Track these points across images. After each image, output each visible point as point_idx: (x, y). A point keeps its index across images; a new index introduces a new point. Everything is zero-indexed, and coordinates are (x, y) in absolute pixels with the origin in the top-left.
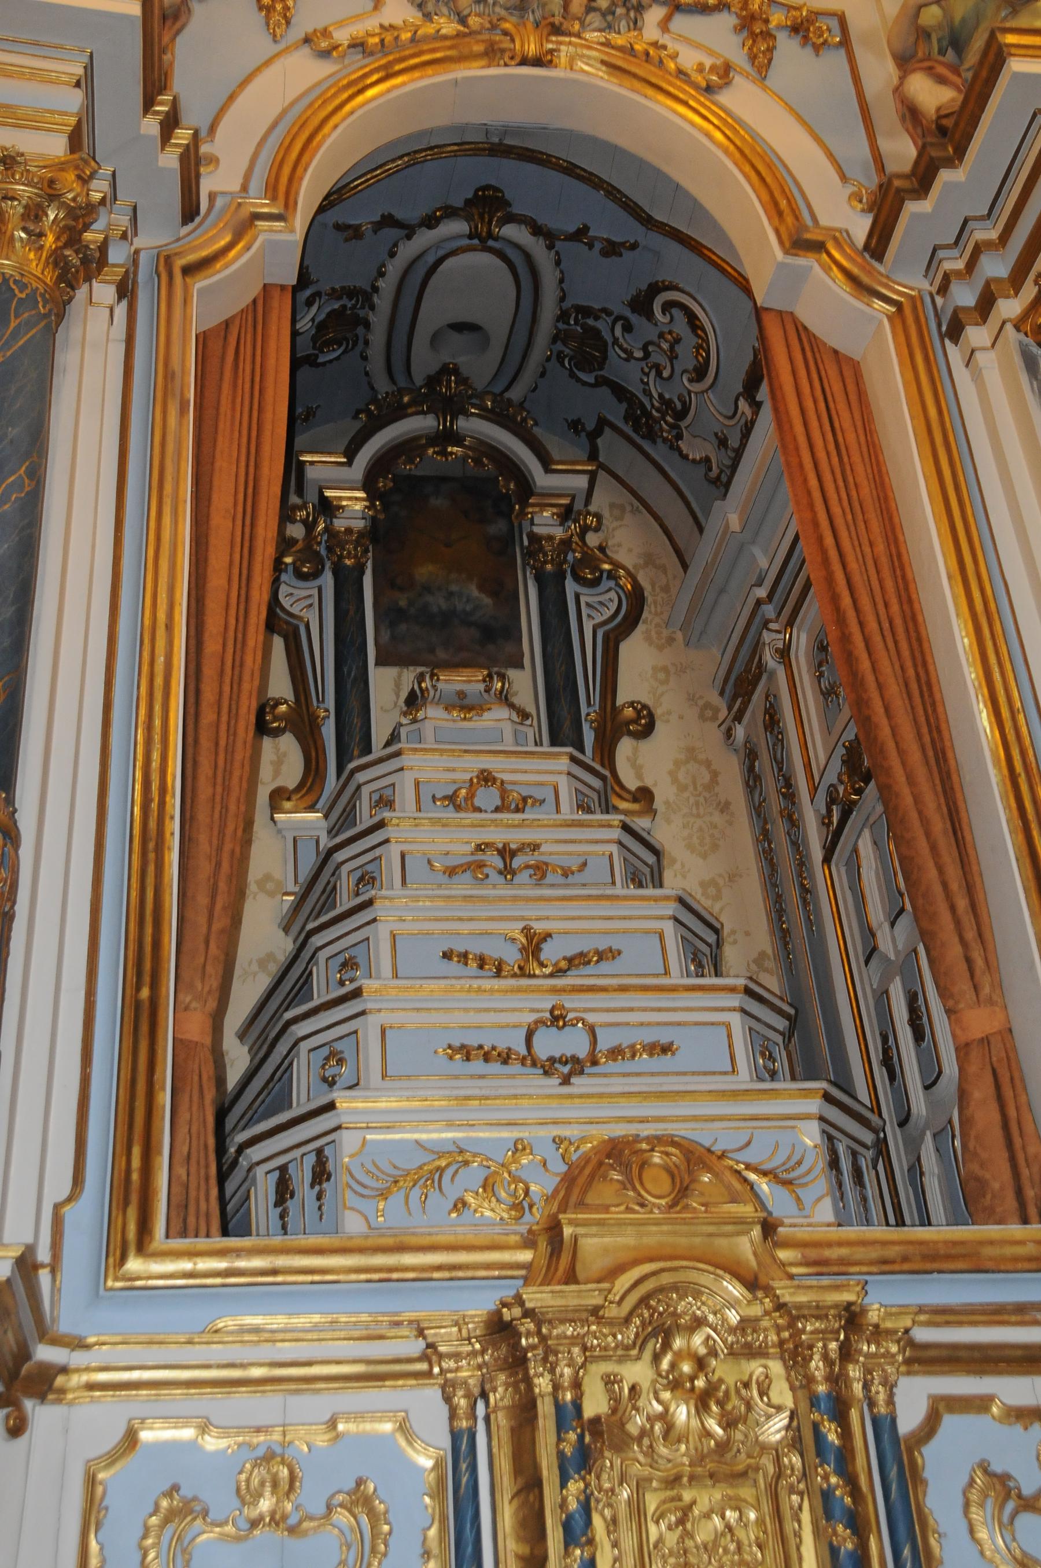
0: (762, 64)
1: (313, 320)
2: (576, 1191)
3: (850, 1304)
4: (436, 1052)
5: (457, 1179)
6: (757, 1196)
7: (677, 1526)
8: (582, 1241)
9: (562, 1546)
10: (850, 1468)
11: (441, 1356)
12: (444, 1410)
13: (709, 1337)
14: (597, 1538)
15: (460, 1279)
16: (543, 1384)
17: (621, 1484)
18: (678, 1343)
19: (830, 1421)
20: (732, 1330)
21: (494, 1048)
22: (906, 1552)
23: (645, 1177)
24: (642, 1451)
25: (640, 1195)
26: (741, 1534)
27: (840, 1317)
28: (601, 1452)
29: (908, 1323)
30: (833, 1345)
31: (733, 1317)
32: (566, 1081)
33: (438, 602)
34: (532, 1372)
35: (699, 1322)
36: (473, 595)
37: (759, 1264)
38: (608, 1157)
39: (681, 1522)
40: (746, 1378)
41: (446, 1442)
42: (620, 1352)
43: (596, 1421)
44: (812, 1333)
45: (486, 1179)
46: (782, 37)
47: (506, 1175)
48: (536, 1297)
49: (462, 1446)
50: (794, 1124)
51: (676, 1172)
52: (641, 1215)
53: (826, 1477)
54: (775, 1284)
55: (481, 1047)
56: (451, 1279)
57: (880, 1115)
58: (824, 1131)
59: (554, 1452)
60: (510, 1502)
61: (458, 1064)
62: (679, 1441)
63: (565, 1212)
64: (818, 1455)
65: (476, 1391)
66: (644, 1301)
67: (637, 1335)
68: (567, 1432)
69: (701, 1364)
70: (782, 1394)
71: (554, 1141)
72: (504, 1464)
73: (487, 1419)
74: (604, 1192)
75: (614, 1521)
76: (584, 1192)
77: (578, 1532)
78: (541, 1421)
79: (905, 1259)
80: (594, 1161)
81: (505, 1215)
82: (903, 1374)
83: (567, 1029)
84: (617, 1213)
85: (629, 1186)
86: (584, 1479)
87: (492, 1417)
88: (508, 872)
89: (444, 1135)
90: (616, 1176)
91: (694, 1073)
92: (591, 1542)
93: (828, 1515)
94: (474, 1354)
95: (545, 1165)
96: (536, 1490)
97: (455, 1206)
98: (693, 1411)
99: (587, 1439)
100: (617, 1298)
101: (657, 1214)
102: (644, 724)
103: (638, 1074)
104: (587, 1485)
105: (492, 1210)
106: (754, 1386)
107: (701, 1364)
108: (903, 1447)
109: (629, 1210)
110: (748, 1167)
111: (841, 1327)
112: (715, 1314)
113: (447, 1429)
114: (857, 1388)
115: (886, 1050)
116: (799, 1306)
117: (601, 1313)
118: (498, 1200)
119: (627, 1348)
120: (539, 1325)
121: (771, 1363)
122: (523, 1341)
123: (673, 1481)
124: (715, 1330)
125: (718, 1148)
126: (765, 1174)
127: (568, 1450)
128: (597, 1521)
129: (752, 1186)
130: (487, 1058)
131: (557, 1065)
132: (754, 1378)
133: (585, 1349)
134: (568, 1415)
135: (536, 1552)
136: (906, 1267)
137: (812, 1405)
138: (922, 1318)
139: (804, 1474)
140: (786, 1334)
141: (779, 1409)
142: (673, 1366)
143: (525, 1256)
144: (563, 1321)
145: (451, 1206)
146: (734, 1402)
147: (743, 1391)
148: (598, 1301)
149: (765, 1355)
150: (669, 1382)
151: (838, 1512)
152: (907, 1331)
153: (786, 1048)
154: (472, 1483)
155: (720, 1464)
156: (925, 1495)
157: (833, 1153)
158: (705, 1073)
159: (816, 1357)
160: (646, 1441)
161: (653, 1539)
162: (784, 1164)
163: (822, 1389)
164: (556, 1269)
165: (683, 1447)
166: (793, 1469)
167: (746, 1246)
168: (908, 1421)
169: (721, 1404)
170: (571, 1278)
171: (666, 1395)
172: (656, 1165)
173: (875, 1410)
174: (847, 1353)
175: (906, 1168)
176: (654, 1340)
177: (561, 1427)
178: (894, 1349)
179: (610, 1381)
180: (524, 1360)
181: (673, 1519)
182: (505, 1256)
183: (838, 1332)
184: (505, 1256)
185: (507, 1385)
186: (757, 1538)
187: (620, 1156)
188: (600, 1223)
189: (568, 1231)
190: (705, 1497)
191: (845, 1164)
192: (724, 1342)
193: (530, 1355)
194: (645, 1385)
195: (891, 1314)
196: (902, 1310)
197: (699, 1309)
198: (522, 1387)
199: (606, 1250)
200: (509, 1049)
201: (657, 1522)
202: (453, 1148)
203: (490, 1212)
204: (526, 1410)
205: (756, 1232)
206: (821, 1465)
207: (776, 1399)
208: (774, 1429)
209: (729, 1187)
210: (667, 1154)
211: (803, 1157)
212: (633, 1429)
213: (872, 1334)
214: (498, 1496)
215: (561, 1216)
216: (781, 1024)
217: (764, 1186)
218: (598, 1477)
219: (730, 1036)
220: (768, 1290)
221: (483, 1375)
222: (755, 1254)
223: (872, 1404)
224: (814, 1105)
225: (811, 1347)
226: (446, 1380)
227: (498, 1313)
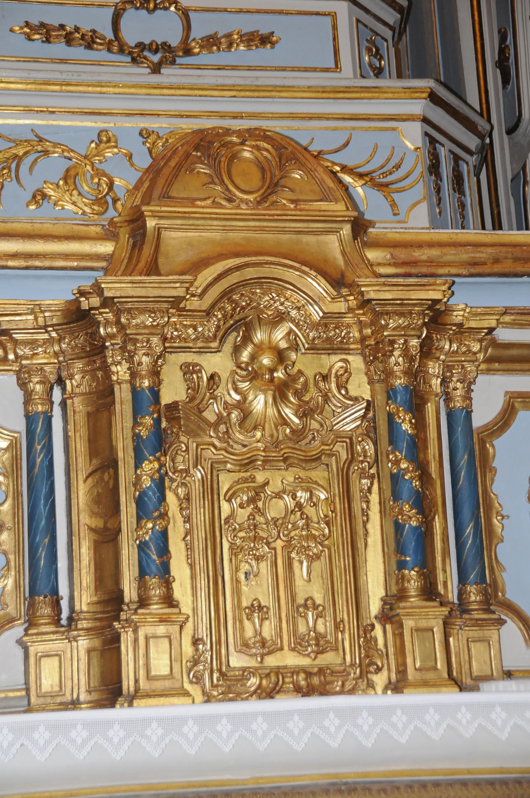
2: (161, 181)
3: (436, 302)
4: (12, 30)
5: (36, 168)
6: (350, 197)
7: (248, 505)
8: (165, 234)
9: (134, 521)
10: (421, 456)
11: (16, 342)
12: (20, 395)
13: (291, 331)
14: (170, 514)
15: (37, 268)
16: (121, 371)
17: (195, 466)
18: (259, 336)
19: (406, 412)
20: (315, 326)
21: (77, 29)
22: (469, 530)
23: (233, 171)
24: (218, 438)
25: (228, 189)
26: (310, 511)
27: (425, 315)
28: (177, 435)
29: (493, 324)
30: (414, 342)
31: (315, 313)
32: (156, 69)
34: (110, 360)
35: (281, 318)
37: (346, 262)
38: (197, 148)
39: (252, 500)
40: (325, 372)
41: (21, 425)
42: (200, 344)
43: (173, 407)
44: (395, 329)
45: (68, 171)
47: (89, 168)
48: (116, 287)
49: (37, 428)
50: (395, 124)
51: (267, 168)
52: (228, 209)
53: (397, 462)
54: (362, 281)
55: (62, 27)
56: (27, 268)
57: (489, 120)
58: (426, 134)
59: (130, 435)
60: (85, 481)
61: (37, 47)
62: (255, 428)
63: (148, 204)
64: (391, 442)
65: (53, 378)
66: (226, 294)
67: (218, 327)
68: (143, 417)
69: (281, 356)
70: (360, 387)
71: (141, 134)
72: (80, 446)
73: (63, 404)
74: (187, 186)
75: (188, 498)
76: (169, 184)
77: (151, 507)
78: (118, 406)
79: (497, 261)
80: (181, 152)
81: (87, 210)
82: (483, 372)
83: (158, 12)
84: (204, 207)
85: (216, 180)
86: (158, 460)
87: (69, 402)
89: (21, 122)
90: (202, 169)
91: (293, 69)
92: (164, 516)
93: (396, 496)
94: (51, 341)
95: (130, 157)
96: (111, 471)
97: (34, 197)
98: (270, 400)
99: (164, 424)
100: (199, 291)
101: (244, 209)
103: (234, 68)
104: (162, 465)
105: (74, 203)
106: (333, 379)
107: (281, 356)
108: (475, 440)
109: (216, 204)
110: (344, 169)
111: (425, 324)
112: (298, 309)
113: (22, 412)
114: (436, 383)
115: (503, 51)
116: (384, 302)
117: (182, 305)
118: (80, 194)
119: (208, 340)
120: (118, 314)
121: (350, 358)
122: (102, 330)
123: (248, 464)
124: (297, 325)
125: (314, 148)
126: (361, 176)
127: (144, 433)
128: (170, 497)
129: (346, 188)
130: (69, 40)
131: (146, 53)
132: (334, 371)
133: (165, 339)
134: (145, 400)
135: (109, 525)
136: (497, 268)
137: (389, 398)
138: (507, 318)
139: (376, 461)
140: (368, 331)
141: (356, 399)
142: (253, 357)
143: (106, 248)
144: (143, 311)
145: (30, 197)
146: (312, 393)
147: (321, 384)
148: (181, 292)
149: (347, 351)
150: (249, 373)
151: (405, 495)
152: (491, 330)
153: (396, 45)
154: (46, 463)
155: (293, 450)
156: (493, 480)
157: (435, 158)
158: (306, 70)
159: (397, 353)
160: (222, 428)
161: (224, 516)
162: (382, 167)
163: (399, 382)
164: (138, 261)
165: (259, 434)
166: (365, 456)
167: (333, 245)
168: (483, 414)
169: (296, 393)
170: (153, 269)
171: (244, 386)
172: (246, 160)
173: (451, 405)
174: (427, 350)
175: (510, 177)
176: (235, 334)
177: (137, 412)
178: (476, 347)
179: (189, 370)
180: (104, 348)
181: (245, 498)
182: (86, 247)
183: (420, 329)
184: (86, 247)
185: (84, 372)
186: (326, 516)
187: (208, 148)
188: (184, 216)
189: (151, 223)
190: (277, 479)
191: (446, 170)
192: (306, 337)
193: (107, 344)
194: (225, 375)
195: (476, 315)
196: (487, 312)
197: (282, 304)
198: (100, 374)
199: (190, 244)
200: (94, 31)
201: (229, 501)
202: (31, 137)
203: (71, 206)
204: (103, 397)
205: (346, 230)
206: (393, 452)
207: (353, 393)
208: (349, 421)
209: (321, 184)
210: (258, 148)
211: (402, 159)
212: (210, 416)
213: (455, 333)
214: (73, 475)
215: (144, 208)
216: (391, 17)
217: (359, 190)
218: (173, 460)
219: (335, 27)
220: (352, 286)
221: (60, 363)
222: (344, 253)
223: (448, 398)
224: (418, 107)
225: (392, 343)
226: (22, 366)
227: (77, 301)
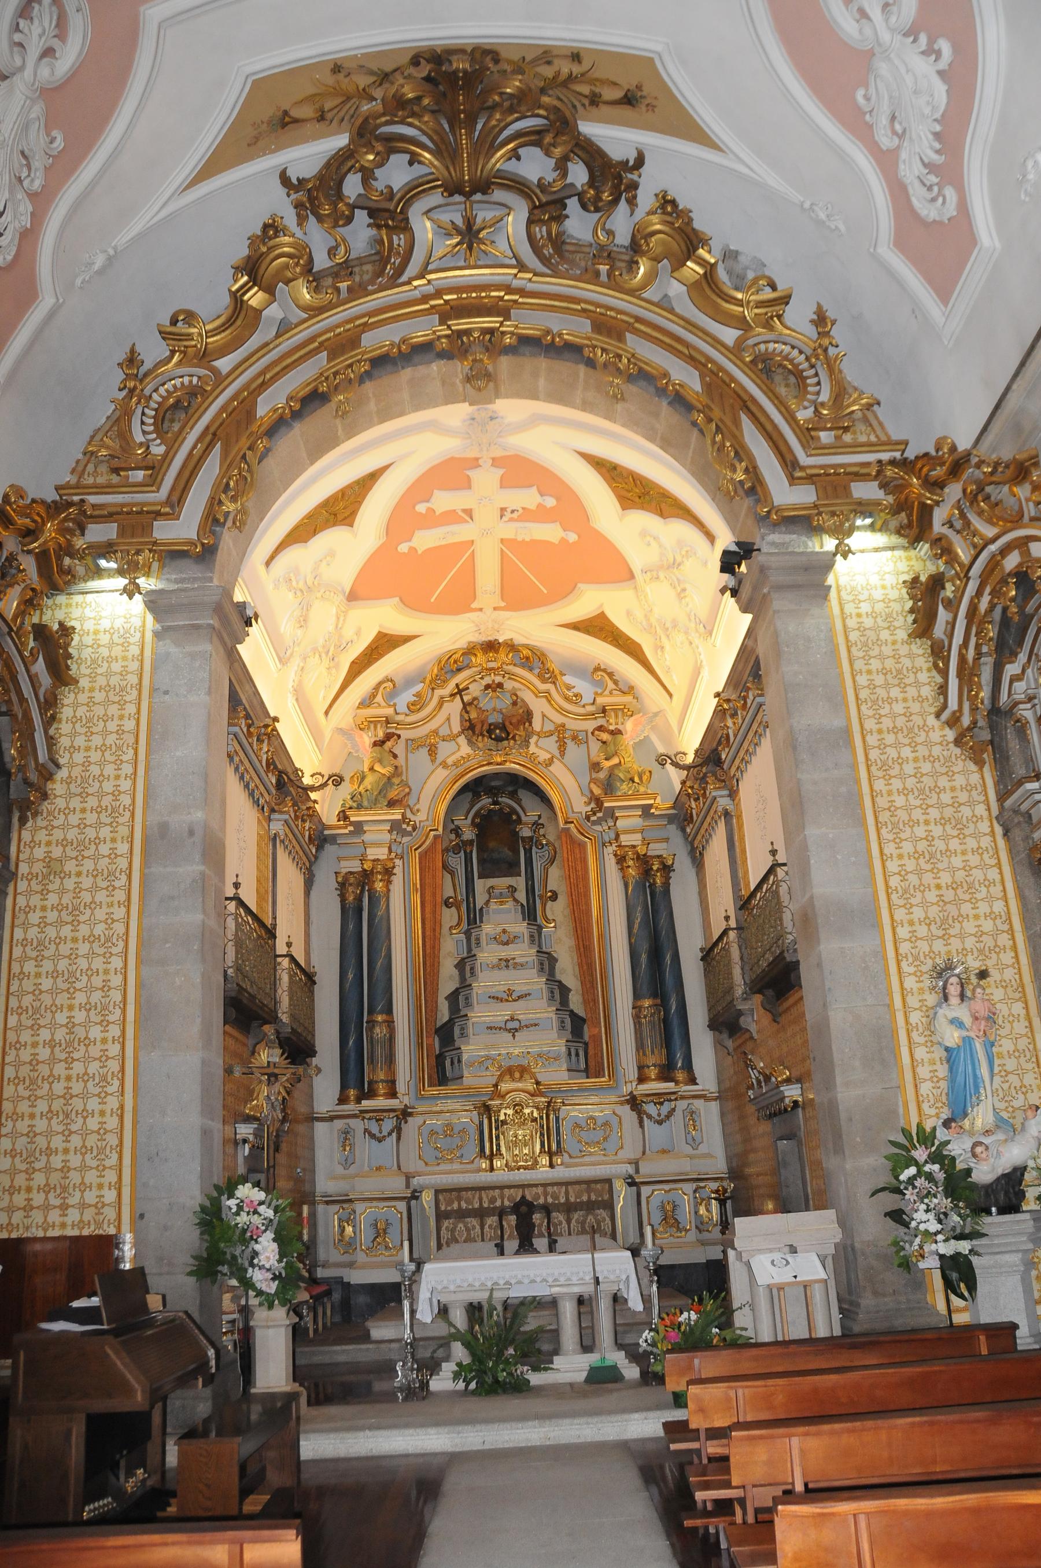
0: (562, 752)
1: (392, 83)
33: (495, 856)
36: (507, 852)
46: (568, 741)
88: (507, 967)
102: (554, 897)
